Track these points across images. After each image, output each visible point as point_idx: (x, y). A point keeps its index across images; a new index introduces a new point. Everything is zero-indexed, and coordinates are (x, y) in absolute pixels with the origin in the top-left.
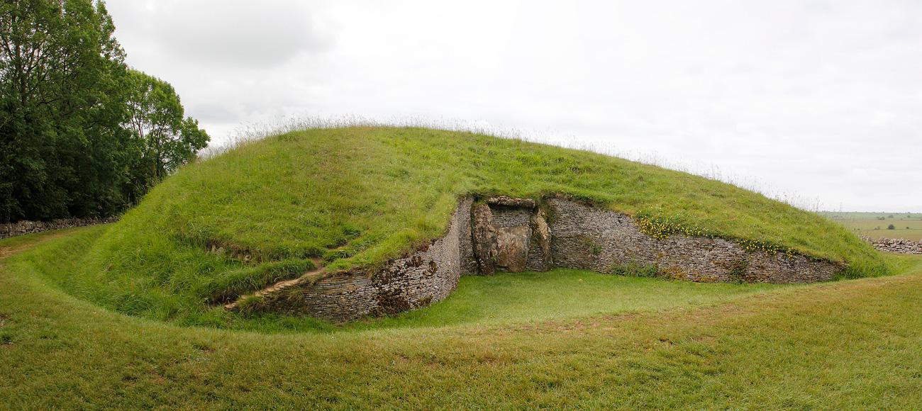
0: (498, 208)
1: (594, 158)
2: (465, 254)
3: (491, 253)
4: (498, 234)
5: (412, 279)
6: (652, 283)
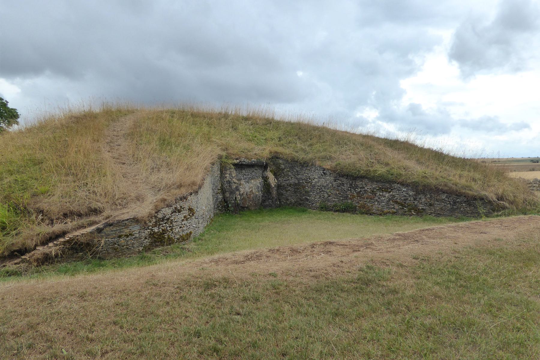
0: (240, 166)
1: (510, 161)
2: (217, 199)
3: (236, 198)
4: (240, 184)
5: (176, 222)
6: (348, 218)
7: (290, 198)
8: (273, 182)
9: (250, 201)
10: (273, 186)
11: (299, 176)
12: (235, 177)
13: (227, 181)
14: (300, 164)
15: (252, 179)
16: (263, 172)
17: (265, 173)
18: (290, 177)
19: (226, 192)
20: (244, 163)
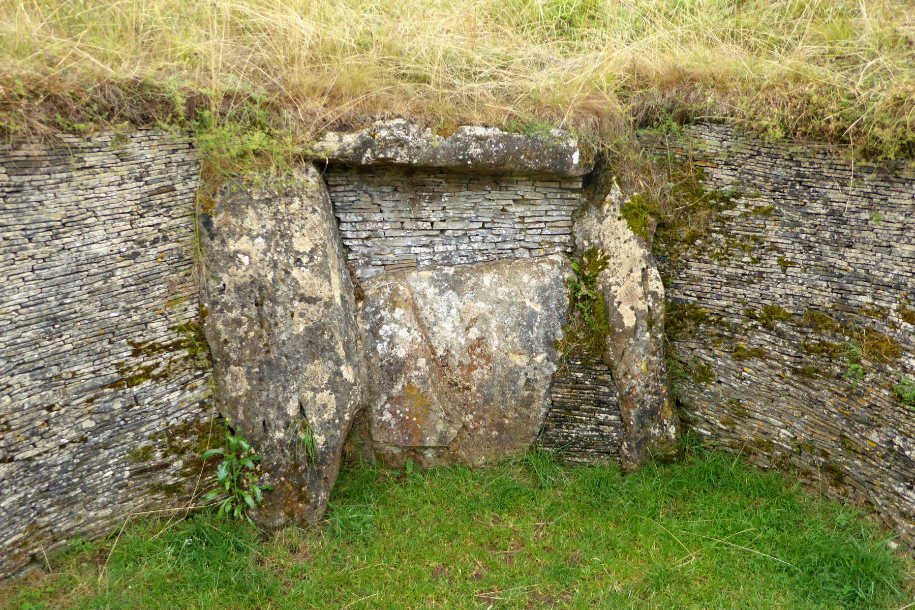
7: (759, 405)
8: (630, 294)
9: (466, 406)
10: (629, 320)
11: (851, 254)
12: (311, 254)
13: (238, 289)
14: (868, 154)
15: (491, 263)
16: (578, 214)
17: (590, 222)
18: (773, 261)
19: (227, 362)
20: (402, 157)
